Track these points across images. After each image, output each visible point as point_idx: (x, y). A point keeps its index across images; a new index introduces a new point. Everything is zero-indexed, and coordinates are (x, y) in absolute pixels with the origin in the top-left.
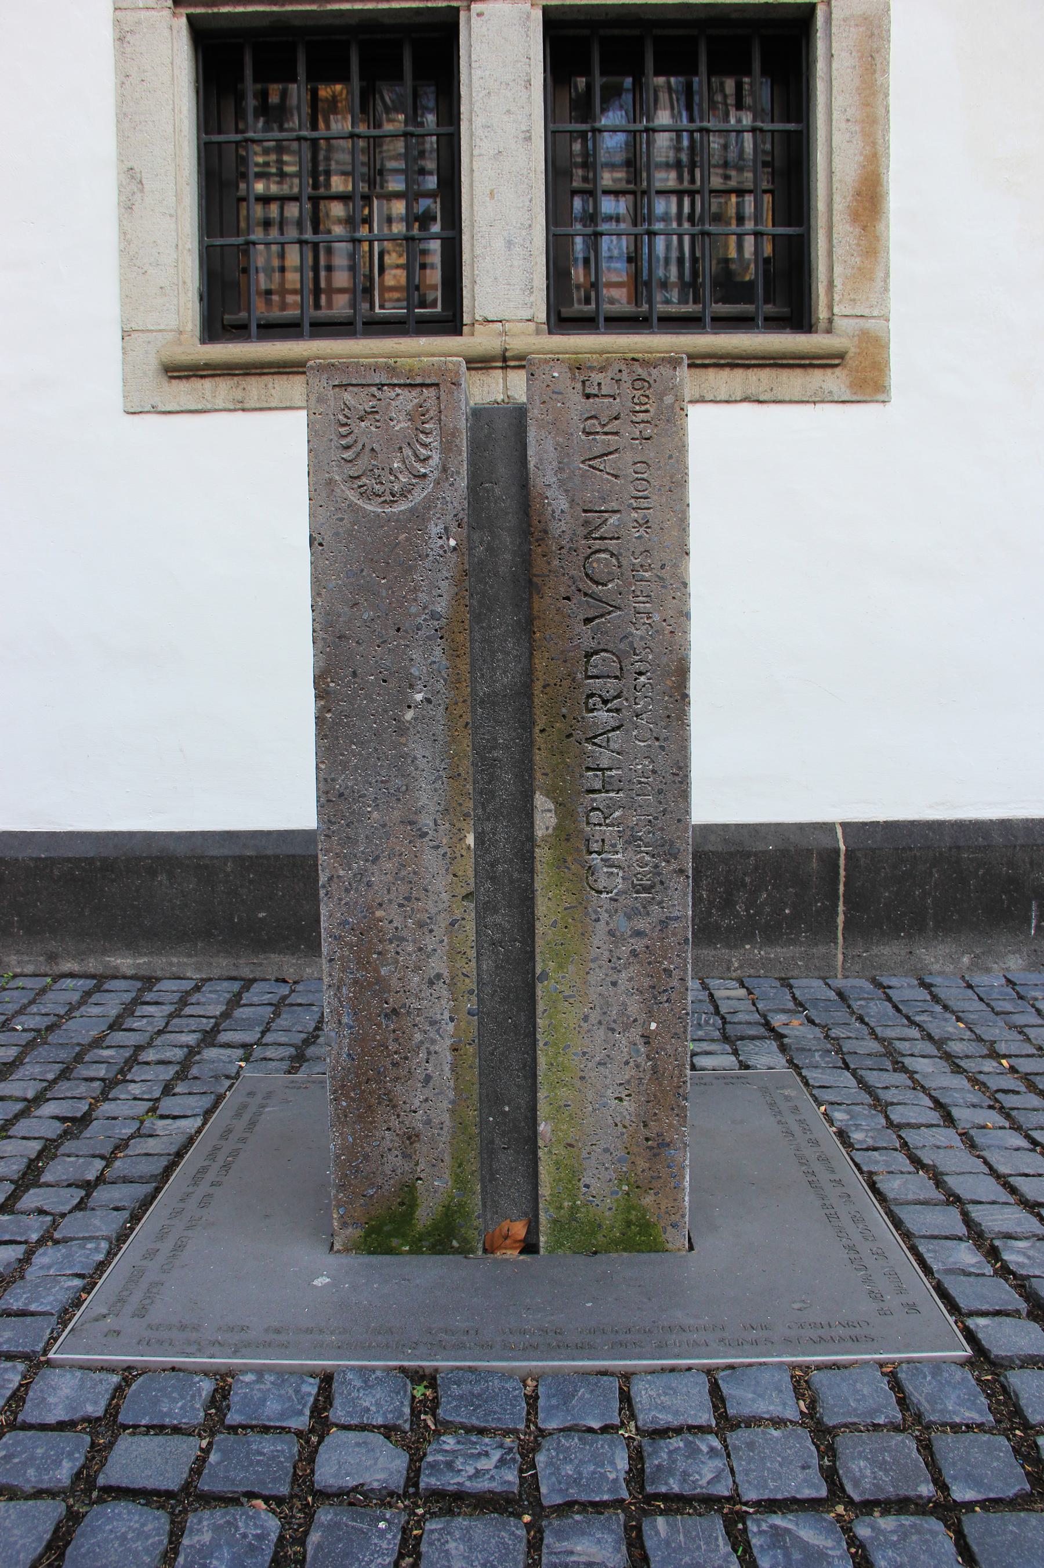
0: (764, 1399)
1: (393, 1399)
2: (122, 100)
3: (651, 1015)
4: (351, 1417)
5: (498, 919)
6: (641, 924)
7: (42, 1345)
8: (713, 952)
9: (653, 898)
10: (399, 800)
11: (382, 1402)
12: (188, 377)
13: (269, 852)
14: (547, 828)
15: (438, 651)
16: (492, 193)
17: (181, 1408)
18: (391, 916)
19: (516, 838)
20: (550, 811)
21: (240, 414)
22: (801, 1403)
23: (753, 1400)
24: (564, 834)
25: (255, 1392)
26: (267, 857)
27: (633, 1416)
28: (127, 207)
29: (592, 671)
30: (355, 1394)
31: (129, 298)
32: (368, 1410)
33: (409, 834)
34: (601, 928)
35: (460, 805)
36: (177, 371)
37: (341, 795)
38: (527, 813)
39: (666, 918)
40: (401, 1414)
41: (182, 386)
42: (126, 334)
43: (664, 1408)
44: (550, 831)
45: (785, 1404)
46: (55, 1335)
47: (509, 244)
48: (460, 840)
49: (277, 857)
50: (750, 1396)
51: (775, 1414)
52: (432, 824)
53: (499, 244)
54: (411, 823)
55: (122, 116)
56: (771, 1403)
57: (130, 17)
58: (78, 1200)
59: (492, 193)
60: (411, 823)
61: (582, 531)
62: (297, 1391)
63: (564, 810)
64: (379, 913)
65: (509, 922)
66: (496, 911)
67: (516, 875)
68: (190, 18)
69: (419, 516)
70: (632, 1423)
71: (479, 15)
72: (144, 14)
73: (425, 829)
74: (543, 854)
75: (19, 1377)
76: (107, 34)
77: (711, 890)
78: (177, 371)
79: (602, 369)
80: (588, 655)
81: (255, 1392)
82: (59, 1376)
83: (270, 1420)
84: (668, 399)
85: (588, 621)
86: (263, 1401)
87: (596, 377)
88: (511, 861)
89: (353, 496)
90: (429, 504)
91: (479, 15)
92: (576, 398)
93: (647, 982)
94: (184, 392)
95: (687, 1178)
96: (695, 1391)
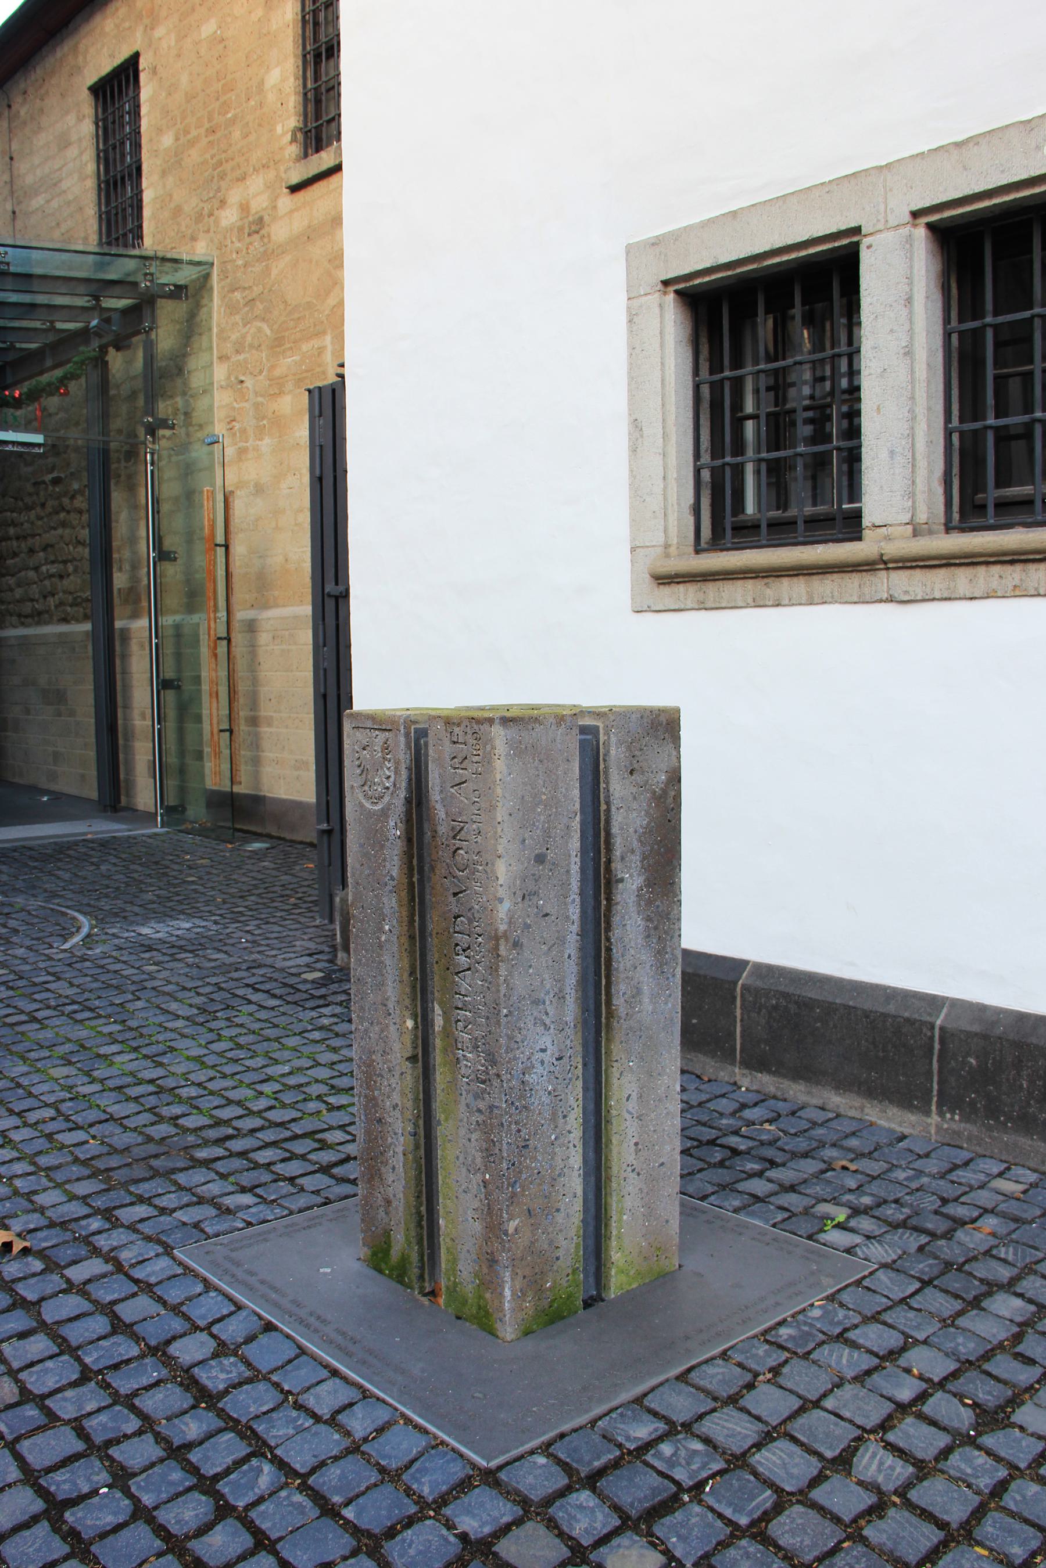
2: (631, 367)
3: (487, 1169)
6: (482, 1105)
8: (1030, 1142)
12: (669, 583)
13: (702, 972)
15: (394, 900)
16: (878, 408)
21: (703, 612)
24: (447, 1033)
26: (699, 976)
28: (634, 450)
29: (457, 929)
31: (635, 523)
34: (463, 1102)
36: (665, 580)
41: (666, 590)
42: (633, 550)
47: (892, 453)
49: (705, 977)
53: (884, 455)
55: (631, 378)
57: (635, 303)
59: (878, 408)
61: (451, 834)
63: (445, 1014)
68: (676, 292)
69: (384, 813)
71: (869, 247)
72: (644, 299)
76: (623, 318)
77: (1032, 1082)
78: (665, 580)
79: (459, 725)
80: (456, 918)
84: (488, 748)
85: (455, 894)
87: (457, 730)
89: (361, 796)
90: (389, 804)
91: (869, 247)
92: (447, 743)
93: (484, 1145)
94: (669, 595)
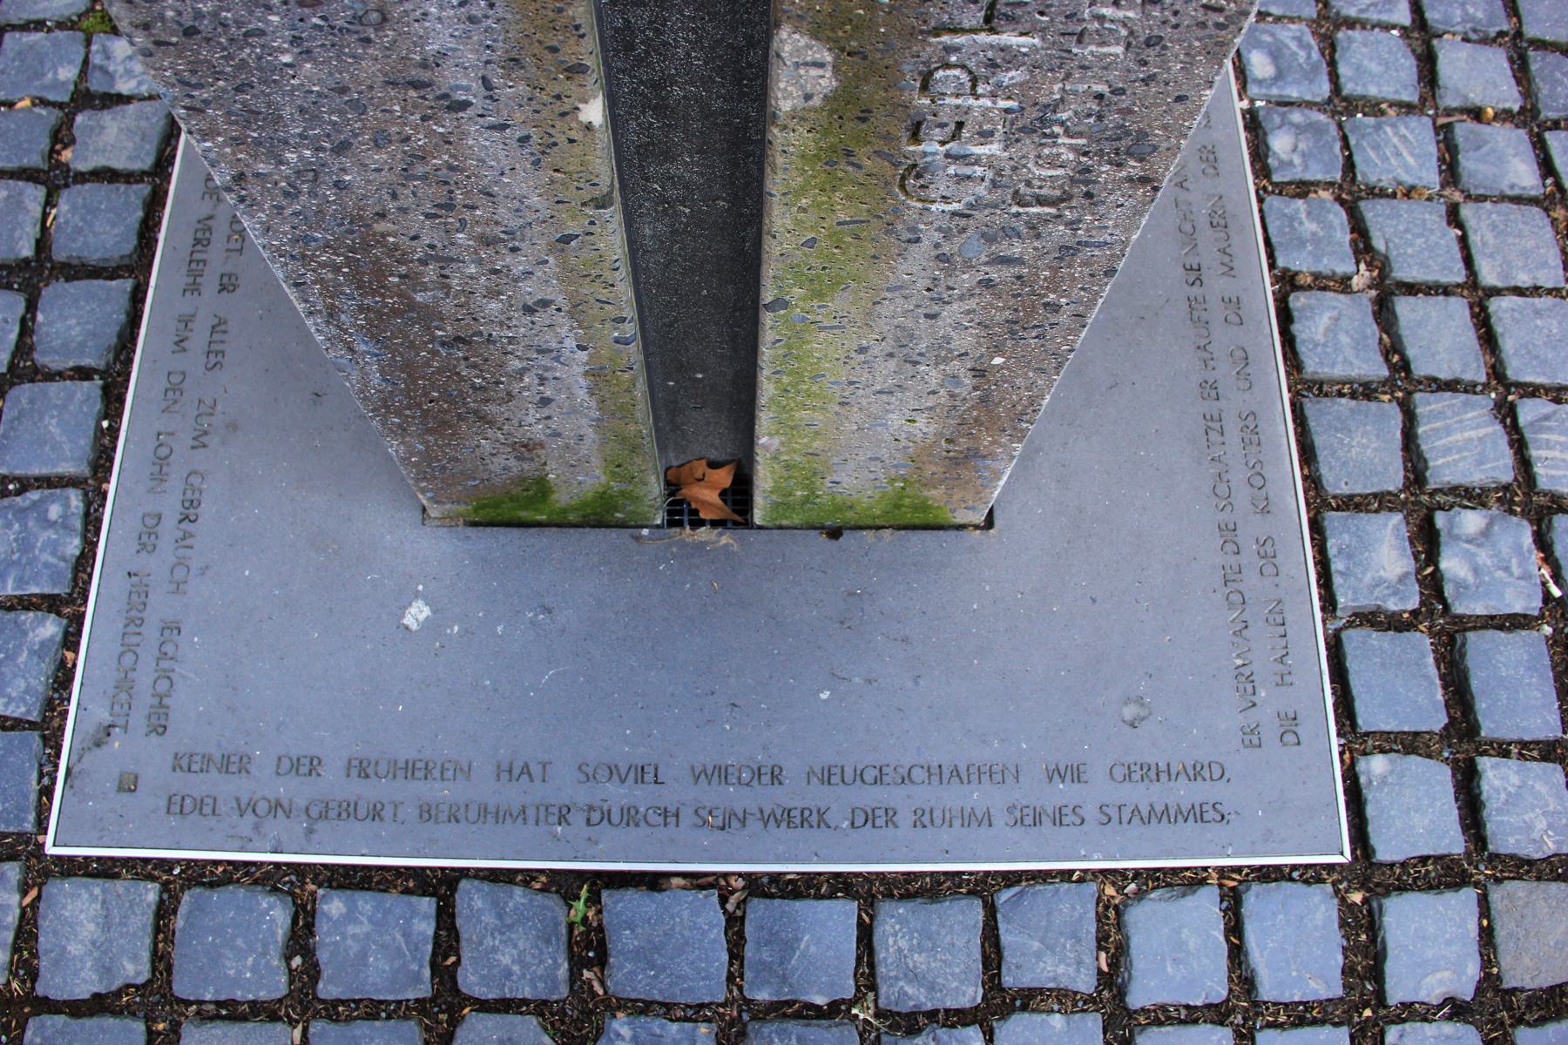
0: (1054, 952)
1: (541, 952)
4: (488, 986)
5: (675, 169)
7: (32, 817)
9: (1059, 216)
10: (368, 41)
11: (528, 958)
14: (808, 97)
17: (254, 969)
18: (412, 227)
19: (719, 42)
20: (821, 65)
22: (1103, 955)
23: (1039, 955)
25: (349, 942)
27: (873, 987)
30: (489, 942)
32: (508, 974)
33: (415, 106)
35: (554, 50)
37: (190, 32)
38: (750, 75)
39: (1079, 243)
40: (554, 980)
43: (914, 977)
44: (817, 101)
45: (1079, 963)
46: (46, 781)
48: (563, 114)
50: (1036, 945)
51: (1064, 983)
52: (476, 86)
54: (416, 85)
56: (1062, 960)
58: (17, 329)
60: (416, 85)
62: (407, 935)
64: (381, 227)
65: (701, 174)
66: (668, 156)
67: (717, 105)
70: (871, 995)
73: (461, 96)
74: (789, 148)
75: (17, 897)
81: (349, 942)
82: (72, 896)
83: (379, 992)
86: (363, 955)
88: (706, 82)
95: (1005, 478)
96: (960, 943)
